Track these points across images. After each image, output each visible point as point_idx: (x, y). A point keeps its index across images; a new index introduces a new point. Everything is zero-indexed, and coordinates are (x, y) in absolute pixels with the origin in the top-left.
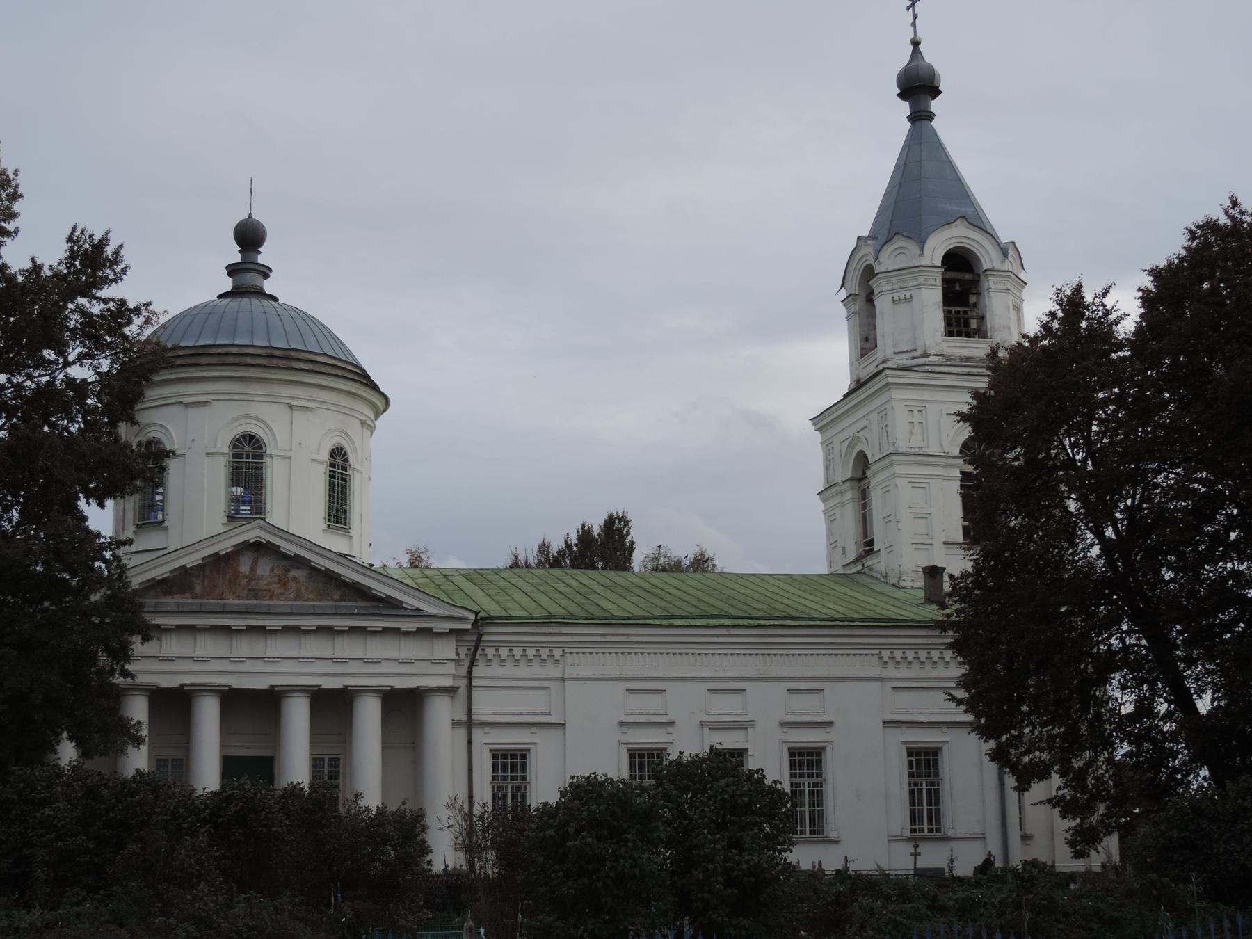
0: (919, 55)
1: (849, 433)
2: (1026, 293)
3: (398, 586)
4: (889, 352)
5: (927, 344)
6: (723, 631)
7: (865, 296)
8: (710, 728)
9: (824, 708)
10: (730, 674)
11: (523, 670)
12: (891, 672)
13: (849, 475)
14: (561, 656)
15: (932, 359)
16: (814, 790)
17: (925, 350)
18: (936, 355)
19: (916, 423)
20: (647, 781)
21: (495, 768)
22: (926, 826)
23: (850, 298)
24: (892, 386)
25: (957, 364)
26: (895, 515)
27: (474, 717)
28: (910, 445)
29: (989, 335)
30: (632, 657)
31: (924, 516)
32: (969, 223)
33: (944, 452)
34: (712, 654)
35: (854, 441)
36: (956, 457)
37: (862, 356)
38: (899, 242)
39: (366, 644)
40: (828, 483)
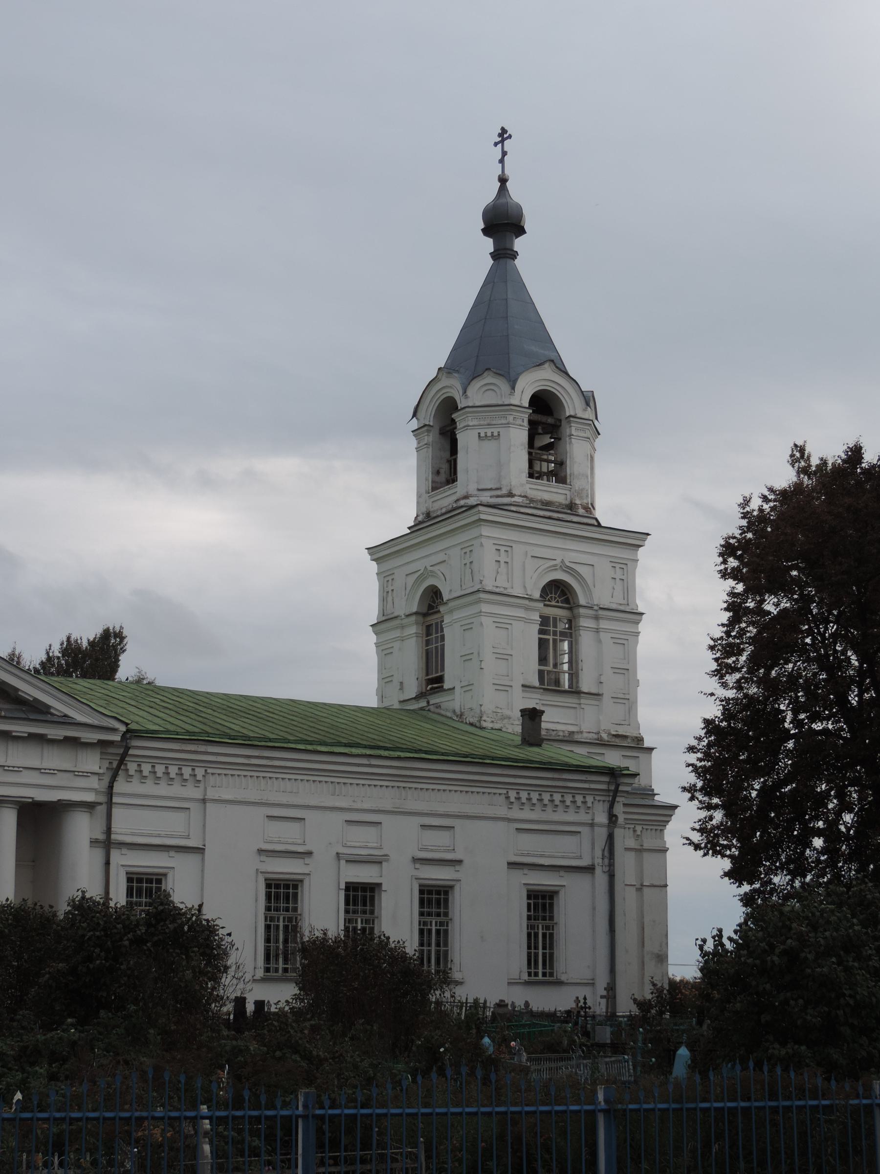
0: (507, 193)
1: (420, 566)
2: (599, 442)
3: (47, 689)
4: (472, 489)
5: (513, 484)
6: (365, 761)
7: (438, 428)
8: (347, 861)
9: (581, 853)
10: (366, 806)
11: (163, 789)
12: (516, 813)
13: (415, 609)
14: (203, 776)
15: (517, 499)
16: (440, 926)
17: (510, 490)
18: (520, 496)
19: (502, 563)
20: (282, 913)
21: (268, 896)
22: (540, 970)
23: (426, 428)
24: (482, 523)
25: (538, 506)
26: (479, 654)
27: (113, 837)
28: (497, 584)
29: (568, 481)
30: (273, 782)
31: (504, 657)
32: (557, 367)
33: (527, 595)
34: (351, 784)
35: (426, 574)
36: (538, 600)
37: (434, 489)
38: (488, 378)
39: (76, 756)
40: (383, 615)
